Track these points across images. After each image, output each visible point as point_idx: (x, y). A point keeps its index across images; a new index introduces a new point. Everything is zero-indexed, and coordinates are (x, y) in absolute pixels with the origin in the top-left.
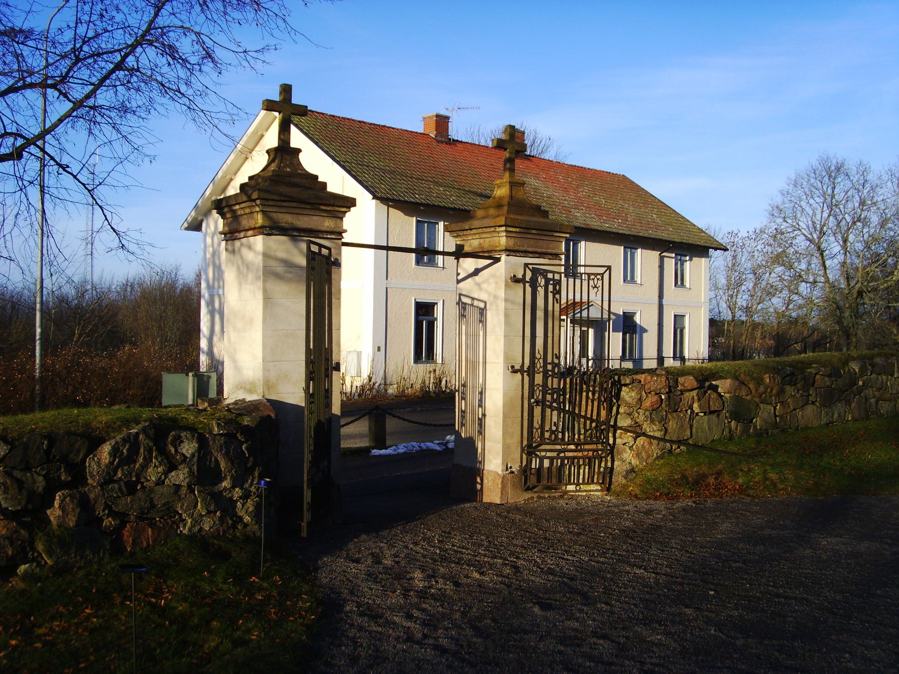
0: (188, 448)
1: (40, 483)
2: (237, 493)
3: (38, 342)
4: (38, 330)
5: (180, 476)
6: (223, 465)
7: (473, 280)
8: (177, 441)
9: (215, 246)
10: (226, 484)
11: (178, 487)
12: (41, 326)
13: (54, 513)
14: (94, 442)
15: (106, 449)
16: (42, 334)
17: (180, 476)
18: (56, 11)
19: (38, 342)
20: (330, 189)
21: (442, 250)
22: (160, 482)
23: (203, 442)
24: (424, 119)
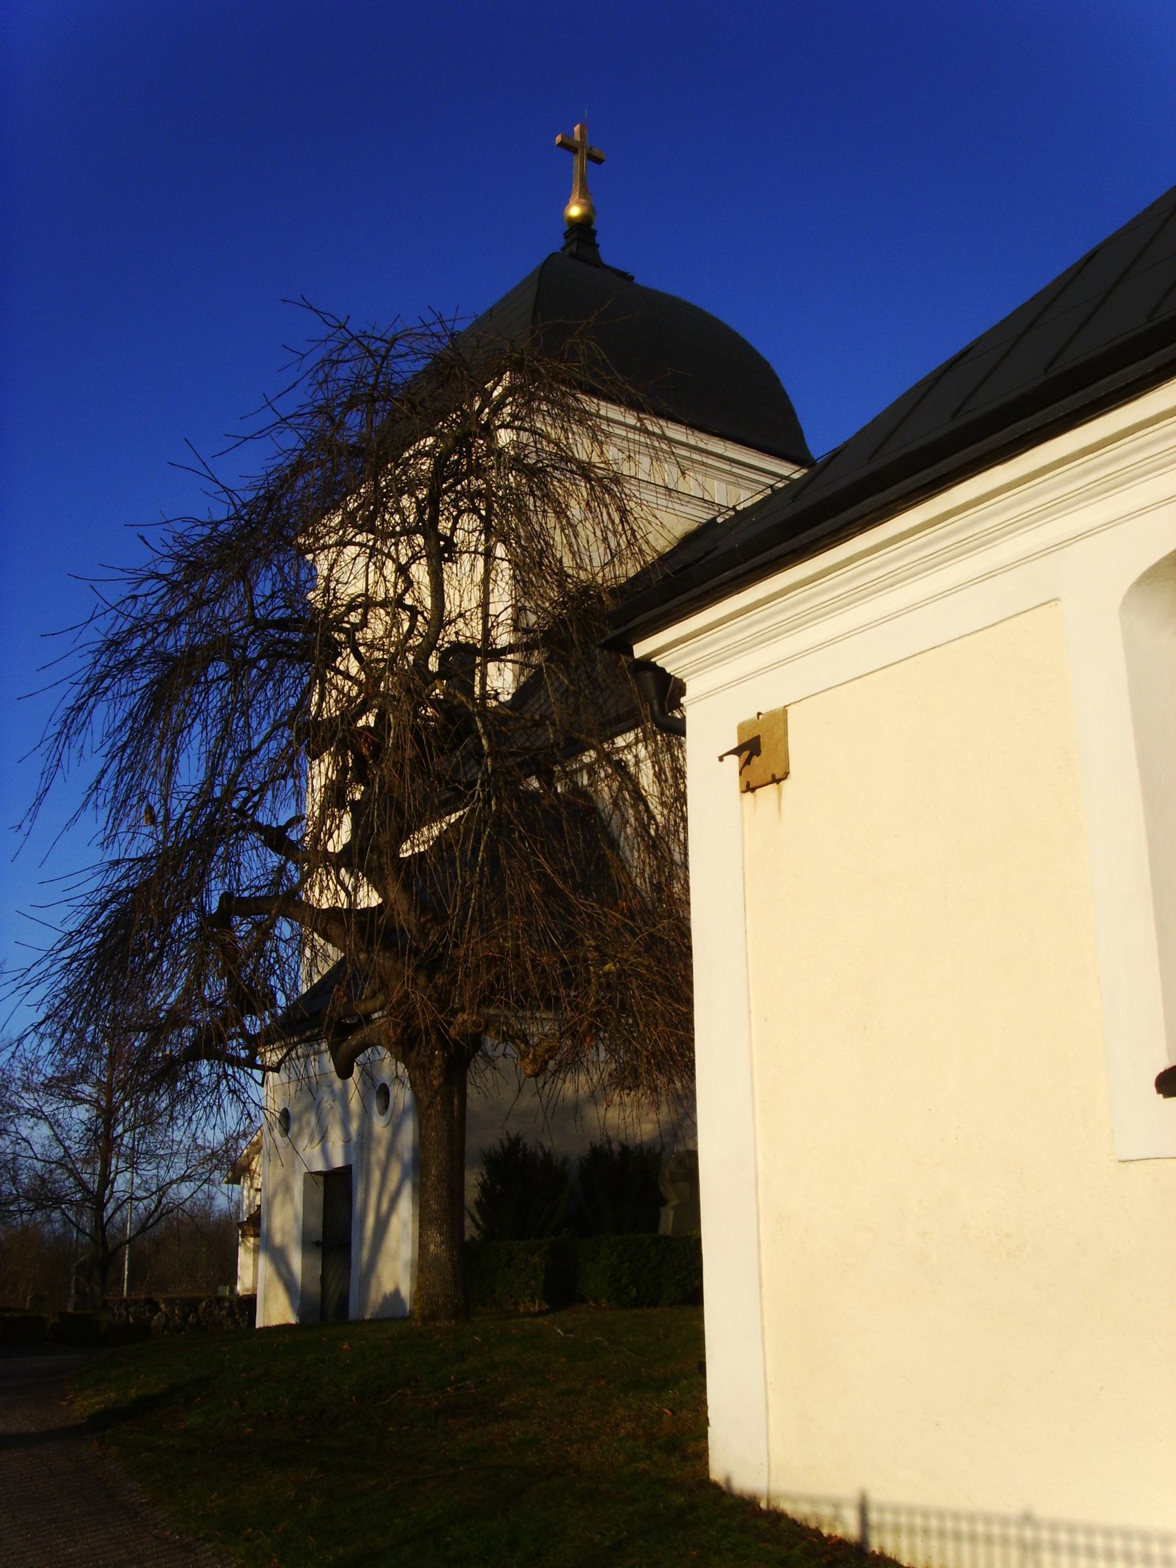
0: (227, 1304)
1: (187, 1310)
2: (241, 1320)
3: (126, 1281)
4: (126, 1273)
5: (224, 1312)
6: (237, 1311)
7: (697, 699)
8: (223, 1303)
9: (251, 1199)
10: (237, 1317)
11: (223, 1316)
12: (128, 1270)
13: (190, 1319)
14: (201, 1300)
15: (204, 1303)
16: (128, 1275)
17: (224, 1312)
18: (53, 717)
19: (126, 1281)
20: (709, 1428)
21: (333, 851)
22: (218, 1314)
23: (231, 1303)
24: (749, 789)
